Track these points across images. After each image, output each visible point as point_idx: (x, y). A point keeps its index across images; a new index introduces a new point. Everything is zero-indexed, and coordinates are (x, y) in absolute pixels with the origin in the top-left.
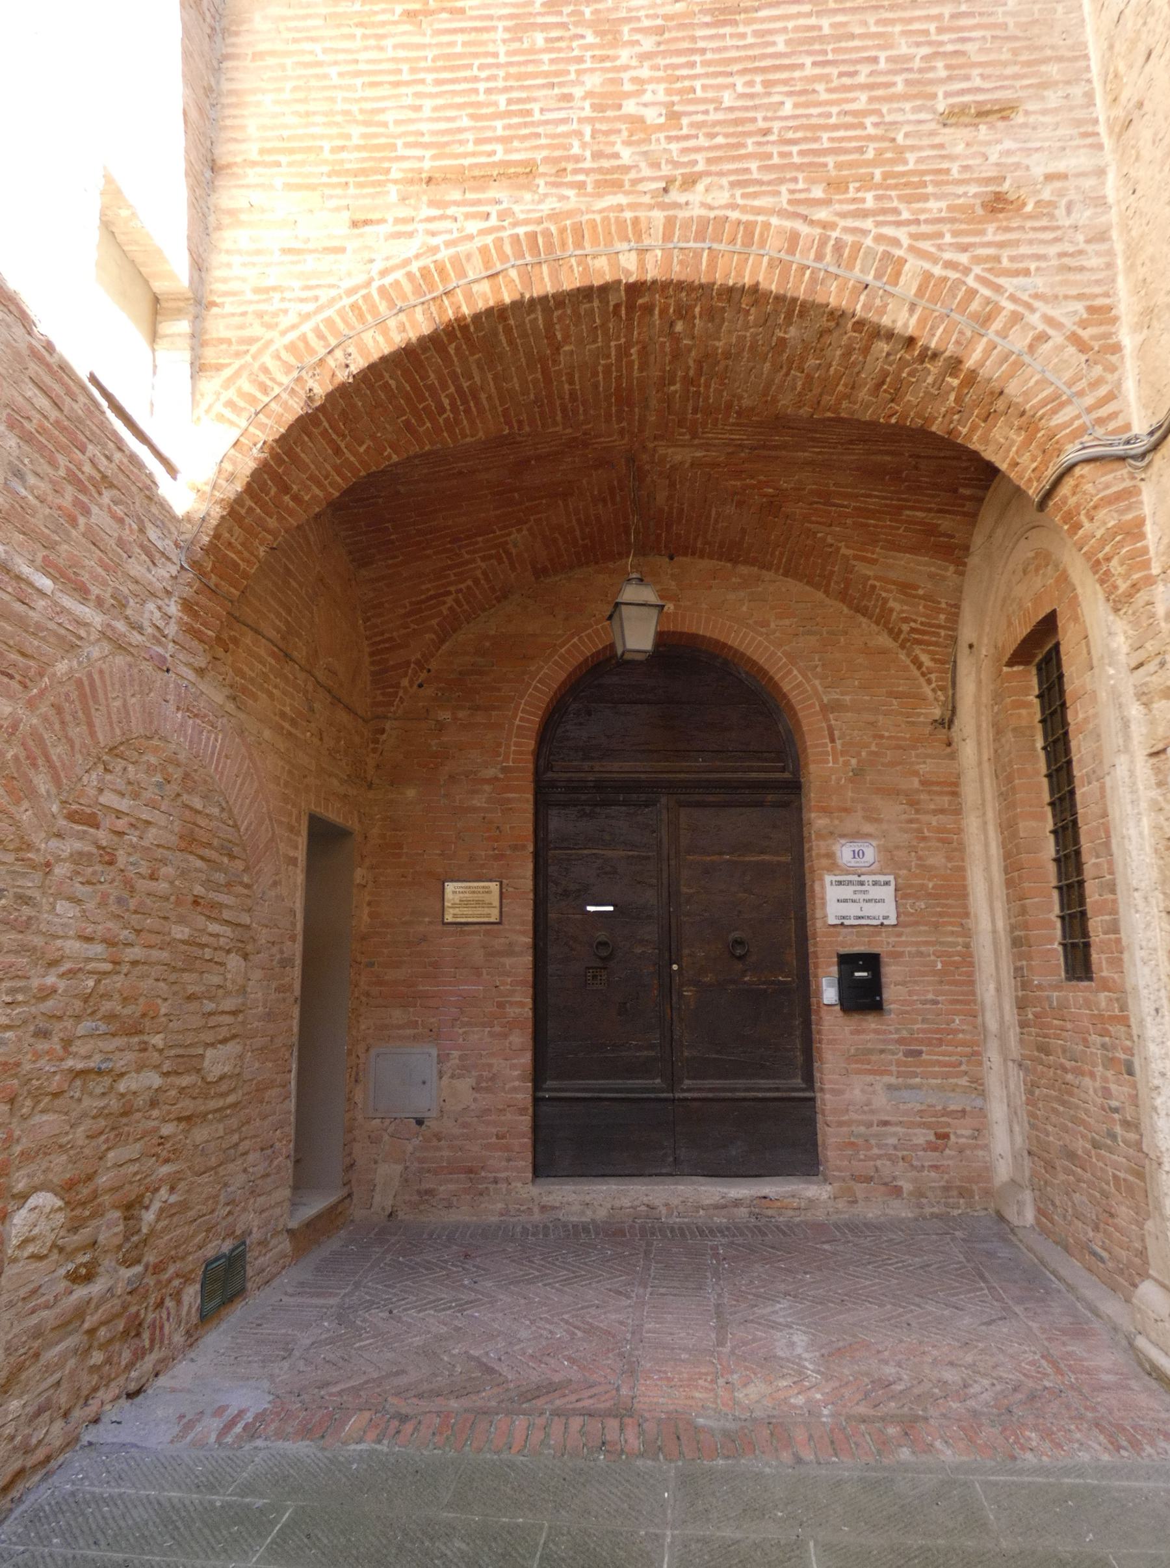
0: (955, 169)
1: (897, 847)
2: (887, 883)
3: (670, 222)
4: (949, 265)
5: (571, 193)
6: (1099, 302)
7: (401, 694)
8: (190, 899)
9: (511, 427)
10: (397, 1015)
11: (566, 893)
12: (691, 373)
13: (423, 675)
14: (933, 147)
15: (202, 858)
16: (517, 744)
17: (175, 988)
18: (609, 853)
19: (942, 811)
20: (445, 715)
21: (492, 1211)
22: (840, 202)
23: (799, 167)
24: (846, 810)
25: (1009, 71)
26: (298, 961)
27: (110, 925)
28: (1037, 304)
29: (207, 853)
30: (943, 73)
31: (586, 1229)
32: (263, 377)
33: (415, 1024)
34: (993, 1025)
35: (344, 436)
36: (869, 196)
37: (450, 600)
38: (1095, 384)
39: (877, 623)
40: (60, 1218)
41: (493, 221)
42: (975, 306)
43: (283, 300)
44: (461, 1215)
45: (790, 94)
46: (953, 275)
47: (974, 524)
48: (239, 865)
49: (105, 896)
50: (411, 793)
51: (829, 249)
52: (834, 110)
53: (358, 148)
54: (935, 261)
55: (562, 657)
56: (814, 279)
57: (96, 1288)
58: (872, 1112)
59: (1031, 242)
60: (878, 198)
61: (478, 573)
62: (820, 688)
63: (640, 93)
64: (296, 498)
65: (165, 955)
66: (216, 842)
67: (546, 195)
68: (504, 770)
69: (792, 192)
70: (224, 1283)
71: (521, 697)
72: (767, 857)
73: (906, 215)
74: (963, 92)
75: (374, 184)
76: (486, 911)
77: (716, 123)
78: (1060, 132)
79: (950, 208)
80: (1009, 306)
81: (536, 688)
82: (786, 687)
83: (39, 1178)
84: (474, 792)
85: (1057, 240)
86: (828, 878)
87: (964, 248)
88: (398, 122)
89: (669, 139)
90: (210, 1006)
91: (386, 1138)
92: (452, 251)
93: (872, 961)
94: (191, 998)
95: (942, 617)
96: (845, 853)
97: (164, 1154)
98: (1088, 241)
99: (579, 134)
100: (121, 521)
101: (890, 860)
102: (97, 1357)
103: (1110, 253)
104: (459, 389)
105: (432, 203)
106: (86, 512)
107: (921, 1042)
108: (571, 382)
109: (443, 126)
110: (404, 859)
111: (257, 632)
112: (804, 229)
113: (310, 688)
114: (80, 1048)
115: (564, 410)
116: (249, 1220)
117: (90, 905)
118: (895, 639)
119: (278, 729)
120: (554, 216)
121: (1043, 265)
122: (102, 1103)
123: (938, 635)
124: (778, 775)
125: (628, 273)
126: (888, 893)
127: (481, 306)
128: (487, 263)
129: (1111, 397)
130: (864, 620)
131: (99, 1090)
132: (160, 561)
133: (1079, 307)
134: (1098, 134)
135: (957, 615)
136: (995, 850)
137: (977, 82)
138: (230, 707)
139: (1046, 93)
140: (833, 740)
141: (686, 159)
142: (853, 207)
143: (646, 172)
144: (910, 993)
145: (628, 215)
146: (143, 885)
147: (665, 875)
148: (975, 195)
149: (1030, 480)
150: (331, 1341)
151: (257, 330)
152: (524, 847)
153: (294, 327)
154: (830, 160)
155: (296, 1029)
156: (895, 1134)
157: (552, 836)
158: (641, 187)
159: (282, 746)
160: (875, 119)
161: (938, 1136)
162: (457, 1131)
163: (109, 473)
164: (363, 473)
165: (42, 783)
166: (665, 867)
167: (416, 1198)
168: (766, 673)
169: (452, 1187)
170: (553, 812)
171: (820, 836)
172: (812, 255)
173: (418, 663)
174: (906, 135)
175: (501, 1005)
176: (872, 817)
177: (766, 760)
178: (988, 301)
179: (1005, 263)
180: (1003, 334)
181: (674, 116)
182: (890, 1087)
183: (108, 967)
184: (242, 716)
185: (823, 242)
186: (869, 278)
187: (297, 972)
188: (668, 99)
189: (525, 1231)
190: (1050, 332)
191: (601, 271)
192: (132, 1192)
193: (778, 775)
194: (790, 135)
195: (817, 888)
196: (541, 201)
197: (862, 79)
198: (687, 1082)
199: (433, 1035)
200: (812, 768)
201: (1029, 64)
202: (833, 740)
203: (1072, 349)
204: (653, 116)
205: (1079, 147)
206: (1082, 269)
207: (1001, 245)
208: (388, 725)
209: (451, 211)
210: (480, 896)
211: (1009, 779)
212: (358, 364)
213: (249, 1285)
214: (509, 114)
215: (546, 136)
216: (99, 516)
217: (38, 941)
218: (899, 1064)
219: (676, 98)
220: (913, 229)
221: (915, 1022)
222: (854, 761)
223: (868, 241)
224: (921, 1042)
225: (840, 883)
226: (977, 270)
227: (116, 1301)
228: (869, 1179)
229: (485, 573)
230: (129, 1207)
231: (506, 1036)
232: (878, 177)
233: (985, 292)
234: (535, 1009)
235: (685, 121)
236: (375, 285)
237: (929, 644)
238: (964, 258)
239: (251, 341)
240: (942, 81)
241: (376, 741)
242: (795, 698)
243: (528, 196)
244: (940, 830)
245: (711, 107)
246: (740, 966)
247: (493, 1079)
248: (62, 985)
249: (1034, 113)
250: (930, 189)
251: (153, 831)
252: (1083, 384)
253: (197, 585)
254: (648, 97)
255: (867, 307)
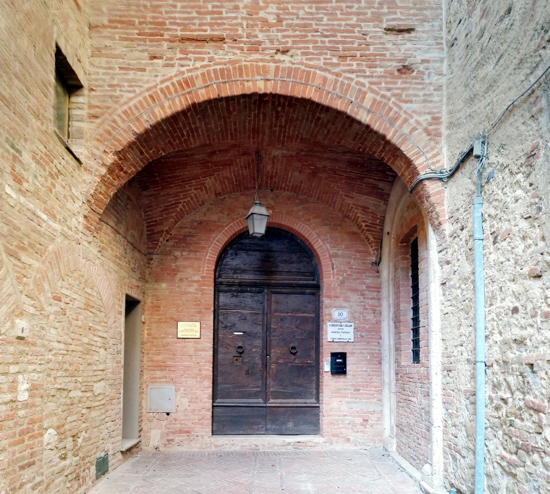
0: (388, 54)
1: (356, 312)
2: (351, 326)
3: (277, 68)
4: (383, 96)
5: (238, 52)
6: (437, 115)
7: (160, 244)
8: (88, 328)
9: (210, 141)
10: (159, 374)
11: (226, 327)
12: (283, 124)
13: (169, 236)
14: (381, 43)
15: (91, 312)
16: (207, 267)
17: (85, 361)
18: (243, 311)
19: (373, 298)
20: (178, 254)
21: (195, 447)
22: (344, 65)
23: (328, 48)
24: (337, 297)
25: (412, 11)
26: (123, 352)
27: (65, 337)
28: (414, 115)
29: (93, 310)
30: (386, 10)
31: (232, 453)
32: (113, 124)
33: (166, 377)
34: (387, 380)
35: (144, 147)
36: (355, 63)
37: (180, 206)
38: (432, 149)
39: (353, 221)
40: (56, 438)
41: (206, 63)
42: (391, 114)
43: (121, 91)
44: (184, 449)
45: (326, 14)
46: (384, 101)
47: (392, 185)
48: (103, 314)
49: (64, 326)
50: (164, 285)
51: (338, 85)
52: (343, 23)
53: (151, 23)
54: (378, 94)
55: (226, 231)
56: (331, 98)
57: (67, 462)
58: (340, 411)
59: (414, 89)
60: (358, 64)
61: (193, 195)
62: (329, 248)
63: (266, 7)
64: (125, 172)
65: (80, 348)
66: (95, 306)
67: (228, 52)
68: (202, 277)
69: (325, 59)
70: (102, 467)
71: (209, 247)
72: (305, 315)
73: (368, 73)
74: (394, 20)
75: (157, 41)
76: (195, 333)
77: (297, 25)
78: (429, 42)
79: (385, 72)
80: (404, 116)
81: (215, 244)
82: (316, 247)
83: (50, 424)
84: (190, 286)
85: (423, 89)
86: (329, 323)
87: (389, 90)
88: (167, 12)
89: (278, 31)
90: (95, 368)
91: (155, 420)
92: (190, 74)
93: (343, 356)
94: (89, 364)
95: (378, 221)
96: (335, 314)
97: (83, 420)
98: (435, 90)
99: (241, 25)
100: (64, 188)
101: (353, 318)
102: (69, 485)
103: (441, 95)
104: (191, 129)
105: (182, 52)
106: (55, 186)
107: (360, 386)
108: (235, 125)
109: (186, 15)
110: (161, 312)
111: (107, 224)
112: (329, 76)
113: (126, 243)
114: (59, 380)
115: (231, 134)
116: (109, 446)
117: (60, 330)
118: (360, 229)
119: (115, 262)
120: (231, 62)
121: (418, 99)
122: (65, 400)
123: (376, 228)
124: (311, 282)
125: (260, 89)
126: (351, 330)
127: (202, 99)
128: (205, 81)
129: (438, 154)
130: (348, 220)
131: (64, 396)
132: (76, 200)
133: (429, 117)
134: (442, 44)
135: (384, 220)
136: (391, 315)
137: (399, 16)
138: (99, 255)
139: (425, 23)
140: (333, 269)
141: (284, 40)
142: (349, 68)
143: (268, 45)
144: (357, 368)
145: (261, 64)
146: (74, 322)
147: (265, 320)
148: (395, 66)
149: (408, 182)
150: (142, 486)
151: (110, 103)
152: (210, 309)
153: (126, 103)
154: (340, 46)
155: (122, 378)
156: (348, 420)
157: (220, 304)
158: (266, 52)
159: (116, 268)
160: (359, 29)
161: (364, 420)
162: (183, 418)
163: (60, 170)
164: (151, 160)
165: (46, 287)
166: (265, 318)
167: (167, 442)
168: (308, 241)
169: (181, 438)
170: (221, 294)
171: (327, 307)
172: (332, 88)
173: (167, 231)
174: (371, 37)
175: (200, 370)
176: (347, 300)
177: (306, 276)
178: (396, 113)
179: (404, 96)
180: (401, 126)
181: (280, 21)
182: (348, 402)
183: (65, 352)
184: (103, 258)
185: (336, 81)
186: (353, 99)
187: (122, 355)
188: (277, 11)
189: (209, 454)
190: (418, 127)
191: (249, 88)
192: (74, 432)
193: (311, 282)
194: (325, 33)
195: (324, 326)
196: (226, 55)
197: (354, 10)
198: (272, 401)
199: (173, 381)
200: (325, 280)
201: (419, 9)
202: (333, 269)
203: (424, 134)
204: (272, 19)
205: (435, 48)
206: (431, 102)
207: (403, 89)
208: (154, 257)
209: (190, 56)
210: (192, 328)
211: (398, 288)
212: (153, 121)
213: (110, 469)
214: (213, 13)
215: (228, 25)
216: (58, 188)
217: (46, 343)
218: (351, 394)
219: (281, 12)
220: (370, 79)
221: (358, 378)
222: (341, 278)
223: (353, 84)
224: (360, 386)
225: (333, 325)
226: (393, 99)
227: (72, 467)
228: (337, 436)
229: (195, 195)
230: (73, 436)
231: (202, 382)
232: (358, 55)
233: (395, 109)
234: (213, 372)
235: (284, 23)
236: (159, 87)
237: (373, 231)
238: (388, 94)
239: (108, 108)
240: (386, 14)
241: (149, 263)
242: (319, 251)
243: (221, 52)
244: (372, 306)
245: (295, 17)
246: (293, 357)
247: (196, 398)
248: (53, 358)
249: (420, 32)
250: (378, 63)
251: (76, 302)
252: (428, 148)
253: (89, 209)
254: (269, 10)
255: (352, 110)
